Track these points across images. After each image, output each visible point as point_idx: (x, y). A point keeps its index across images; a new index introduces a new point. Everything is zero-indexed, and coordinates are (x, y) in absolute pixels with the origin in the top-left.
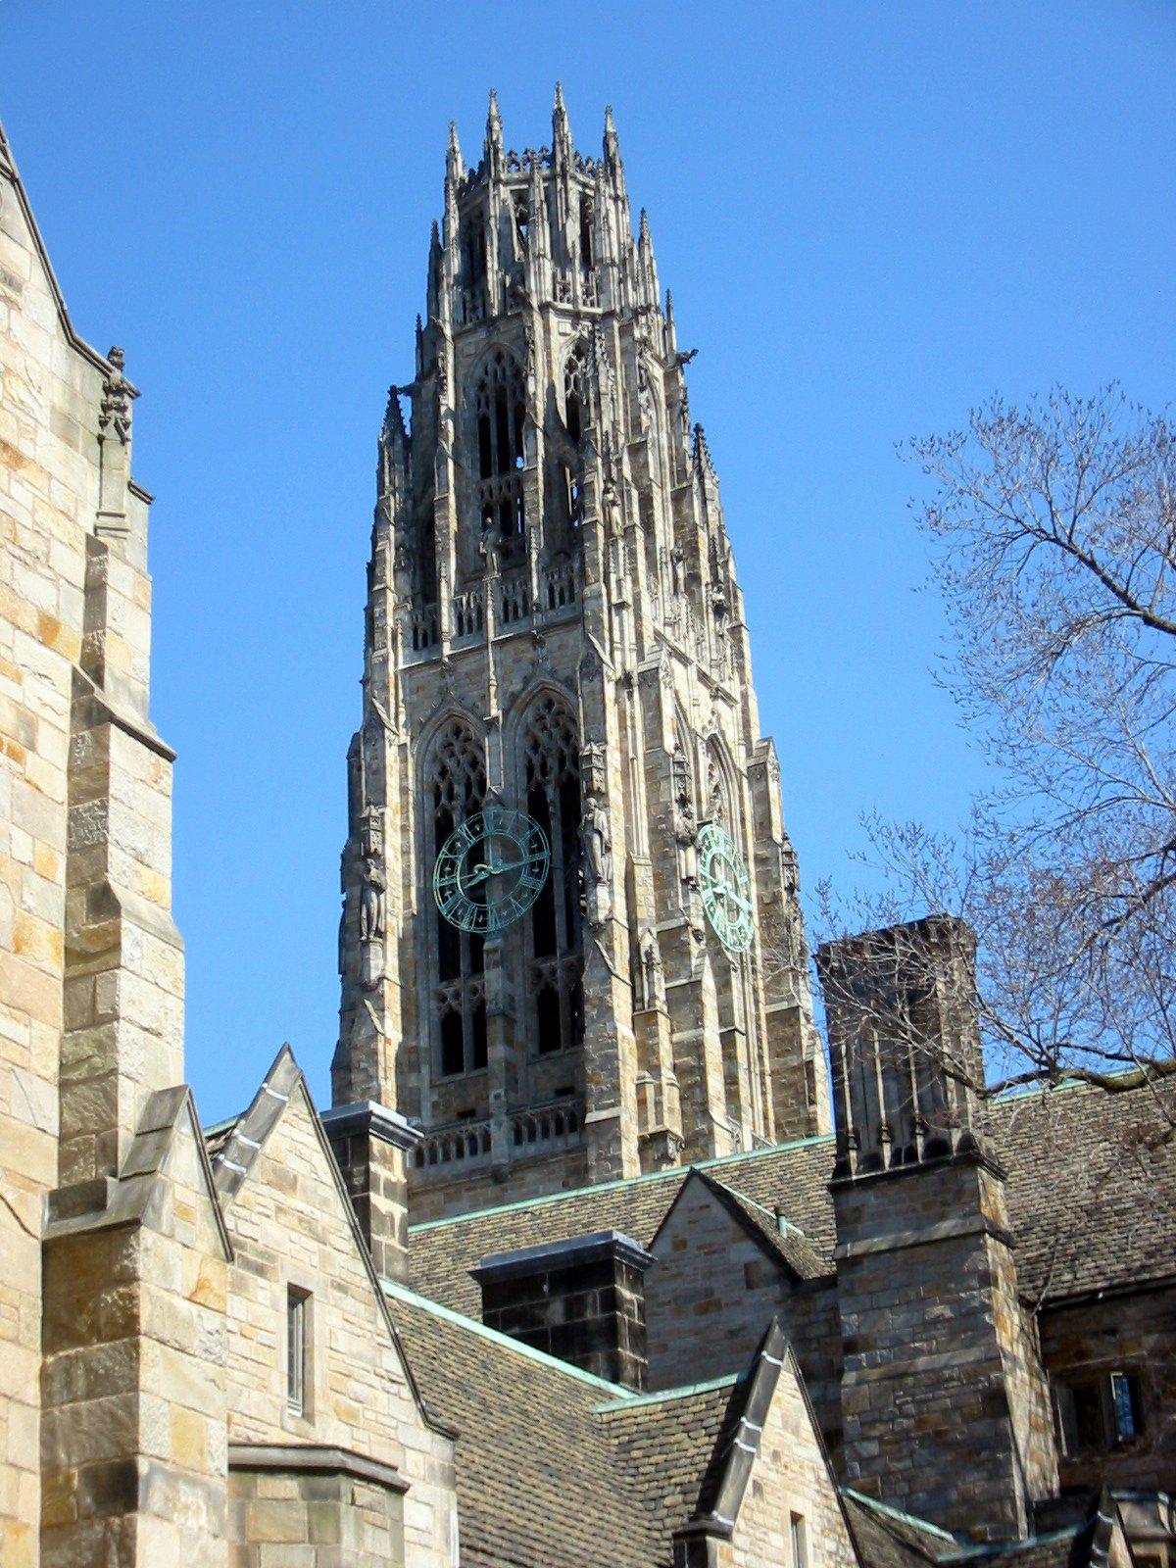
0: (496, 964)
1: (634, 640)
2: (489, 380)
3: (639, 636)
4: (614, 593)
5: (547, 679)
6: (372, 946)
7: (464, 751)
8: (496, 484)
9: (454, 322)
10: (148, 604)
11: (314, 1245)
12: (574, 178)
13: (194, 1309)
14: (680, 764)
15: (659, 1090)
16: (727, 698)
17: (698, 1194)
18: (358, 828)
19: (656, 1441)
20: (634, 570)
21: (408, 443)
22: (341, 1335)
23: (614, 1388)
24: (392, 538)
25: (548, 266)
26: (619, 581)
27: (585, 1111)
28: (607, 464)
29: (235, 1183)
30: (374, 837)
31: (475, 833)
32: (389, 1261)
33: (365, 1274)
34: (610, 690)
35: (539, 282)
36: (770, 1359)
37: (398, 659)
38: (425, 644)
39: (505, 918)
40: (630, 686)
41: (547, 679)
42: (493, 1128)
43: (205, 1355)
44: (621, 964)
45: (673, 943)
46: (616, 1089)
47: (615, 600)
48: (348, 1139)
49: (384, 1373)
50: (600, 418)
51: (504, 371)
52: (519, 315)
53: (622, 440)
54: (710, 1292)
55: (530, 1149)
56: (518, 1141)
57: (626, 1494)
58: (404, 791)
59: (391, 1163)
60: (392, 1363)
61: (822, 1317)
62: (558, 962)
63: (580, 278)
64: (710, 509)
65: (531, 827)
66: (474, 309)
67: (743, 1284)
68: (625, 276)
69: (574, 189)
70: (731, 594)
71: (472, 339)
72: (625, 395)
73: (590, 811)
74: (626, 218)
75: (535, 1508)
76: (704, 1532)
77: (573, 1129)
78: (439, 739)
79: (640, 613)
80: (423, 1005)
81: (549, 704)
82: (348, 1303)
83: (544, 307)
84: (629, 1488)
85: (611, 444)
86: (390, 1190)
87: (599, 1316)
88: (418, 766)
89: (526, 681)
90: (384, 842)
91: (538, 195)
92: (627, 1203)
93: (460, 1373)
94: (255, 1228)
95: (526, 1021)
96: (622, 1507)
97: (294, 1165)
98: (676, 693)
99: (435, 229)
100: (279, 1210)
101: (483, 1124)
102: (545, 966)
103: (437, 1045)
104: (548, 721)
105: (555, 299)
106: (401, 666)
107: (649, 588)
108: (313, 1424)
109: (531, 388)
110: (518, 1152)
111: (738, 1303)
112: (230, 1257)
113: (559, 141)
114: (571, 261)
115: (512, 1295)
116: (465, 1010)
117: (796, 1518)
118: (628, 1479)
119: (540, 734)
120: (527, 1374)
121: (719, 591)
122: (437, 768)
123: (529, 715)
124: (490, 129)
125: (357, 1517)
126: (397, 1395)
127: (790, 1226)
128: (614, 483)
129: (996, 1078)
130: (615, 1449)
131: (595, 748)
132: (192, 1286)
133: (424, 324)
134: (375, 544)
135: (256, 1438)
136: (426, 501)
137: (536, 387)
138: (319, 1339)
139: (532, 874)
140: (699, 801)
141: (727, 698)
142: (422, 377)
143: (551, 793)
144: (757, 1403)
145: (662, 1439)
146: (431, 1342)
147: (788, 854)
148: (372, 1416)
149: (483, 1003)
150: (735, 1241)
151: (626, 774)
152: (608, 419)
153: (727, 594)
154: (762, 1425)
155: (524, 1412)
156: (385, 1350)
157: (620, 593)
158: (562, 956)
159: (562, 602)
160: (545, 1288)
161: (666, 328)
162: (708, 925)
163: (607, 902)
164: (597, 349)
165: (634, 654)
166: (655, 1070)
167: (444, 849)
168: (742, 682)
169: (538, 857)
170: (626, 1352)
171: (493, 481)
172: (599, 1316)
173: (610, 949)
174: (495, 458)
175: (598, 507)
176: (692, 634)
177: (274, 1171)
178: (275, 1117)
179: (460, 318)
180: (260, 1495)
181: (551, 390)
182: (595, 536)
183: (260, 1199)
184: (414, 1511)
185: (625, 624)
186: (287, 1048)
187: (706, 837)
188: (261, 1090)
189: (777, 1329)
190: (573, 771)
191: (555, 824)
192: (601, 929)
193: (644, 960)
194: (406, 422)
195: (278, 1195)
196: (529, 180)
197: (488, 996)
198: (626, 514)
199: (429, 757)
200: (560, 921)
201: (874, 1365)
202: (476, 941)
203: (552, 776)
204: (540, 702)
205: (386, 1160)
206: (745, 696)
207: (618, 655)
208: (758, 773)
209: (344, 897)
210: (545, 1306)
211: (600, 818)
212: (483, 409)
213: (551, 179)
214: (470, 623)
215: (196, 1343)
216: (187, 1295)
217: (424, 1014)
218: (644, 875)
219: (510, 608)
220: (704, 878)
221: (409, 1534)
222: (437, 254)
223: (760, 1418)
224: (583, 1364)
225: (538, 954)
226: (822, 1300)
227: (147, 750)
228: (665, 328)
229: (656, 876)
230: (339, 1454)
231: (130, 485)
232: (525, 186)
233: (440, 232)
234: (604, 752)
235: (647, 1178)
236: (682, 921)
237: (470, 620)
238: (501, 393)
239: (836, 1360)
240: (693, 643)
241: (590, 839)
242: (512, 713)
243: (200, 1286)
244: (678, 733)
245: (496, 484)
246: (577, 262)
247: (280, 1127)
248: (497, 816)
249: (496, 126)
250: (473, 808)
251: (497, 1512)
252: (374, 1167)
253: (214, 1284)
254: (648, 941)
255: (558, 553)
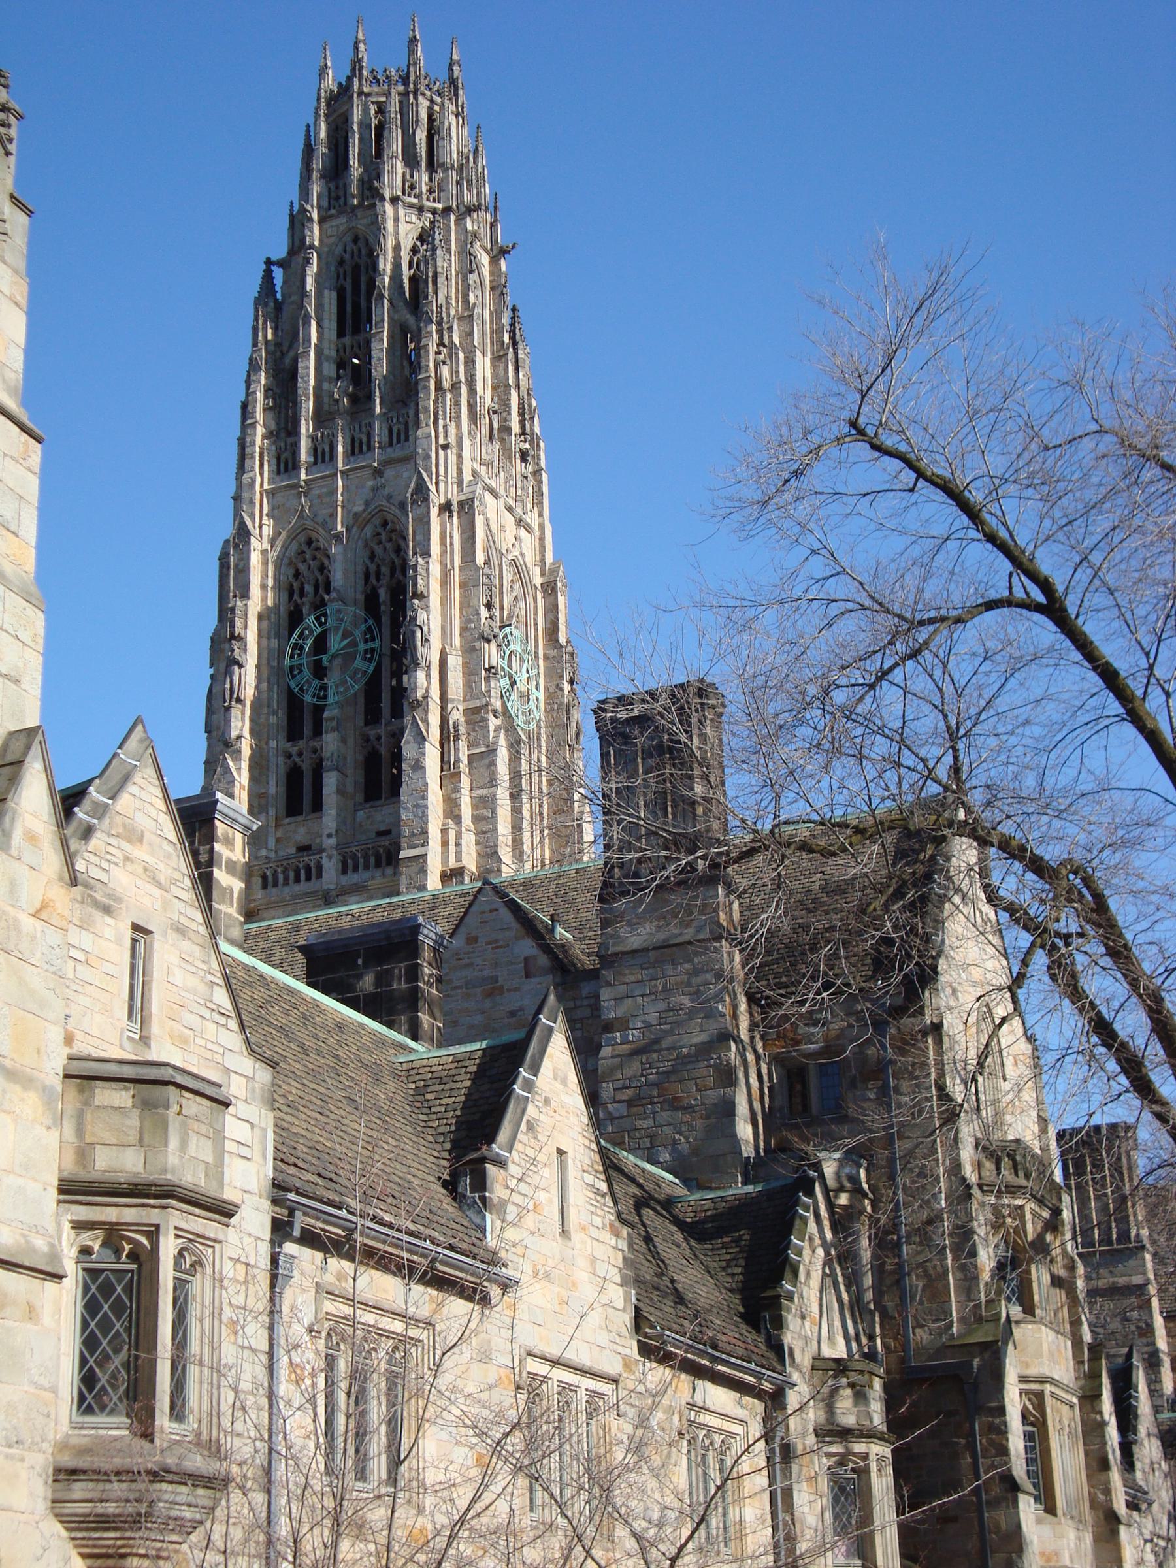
0: (333, 730)
1: (455, 475)
2: (347, 257)
3: (460, 471)
4: (441, 436)
5: (384, 503)
6: (233, 711)
7: (314, 558)
8: (348, 351)
9: (319, 208)
10: (24, 302)
11: (157, 892)
12: (423, 94)
13: (39, 924)
14: (489, 576)
15: (459, 835)
16: (528, 528)
17: (489, 896)
18: (226, 614)
19: (447, 1087)
20: (458, 418)
21: (279, 307)
22: (177, 971)
23: (412, 1044)
24: (263, 382)
25: (399, 166)
26: (445, 426)
27: (399, 849)
28: (440, 332)
29: (87, 833)
30: (238, 622)
31: (321, 624)
32: (227, 927)
33: (201, 920)
34: (434, 512)
35: (391, 179)
36: (544, 1020)
37: (262, 478)
38: (286, 470)
39: (341, 690)
40: (451, 512)
41: (384, 503)
42: (325, 861)
43: (46, 967)
44: (434, 734)
45: (476, 716)
46: (424, 832)
47: (441, 441)
48: (196, 820)
49: (215, 1007)
50: (436, 293)
51: (360, 251)
52: (374, 205)
53: (453, 312)
54: (495, 979)
55: (354, 878)
56: (344, 871)
57: (419, 1129)
58: (264, 587)
59: (233, 845)
60: (222, 998)
61: (585, 1002)
62: (382, 730)
63: (425, 178)
64: (521, 374)
65: (366, 621)
66: (337, 198)
67: (523, 974)
68: (462, 179)
69: (424, 103)
70: (534, 441)
71: (334, 222)
72: (457, 275)
73: (414, 610)
74: (465, 131)
75: (341, 1134)
76: (483, 1160)
77: (389, 863)
78: (294, 546)
79: (459, 455)
80: (273, 759)
81: (385, 524)
82: (186, 945)
83: (395, 200)
84: (422, 1124)
85: (444, 315)
86: (231, 867)
87: (404, 986)
88: (277, 569)
89: (367, 504)
90: (246, 628)
91: (394, 108)
92: (431, 909)
93: (284, 1021)
94: (104, 873)
95: (355, 776)
96: (415, 1139)
97: (143, 822)
98: (487, 520)
99: (308, 131)
100: (127, 859)
101: (317, 857)
102: (372, 733)
103: (282, 789)
104: (383, 537)
105: (404, 194)
106: (266, 486)
107: (469, 433)
108: (149, 1047)
109: (381, 266)
110: (344, 880)
111: (517, 989)
112: (74, 881)
113: (412, 62)
114: (418, 163)
115: (329, 965)
116: (306, 766)
117: (560, 1152)
118: (422, 1117)
119: (376, 547)
120: (341, 1026)
121: (525, 441)
122: (291, 572)
123: (368, 531)
124: (357, 48)
125: (184, 1125)
126: (226, 1026)
127: (563, 931)
128: (445, 346)
129: (742, 798)
130: (412, 1092)
131: (420, 560)
132: (38, 905)
133: (296, 208)
134: (248, 386)
135: (96, 1053)
136: (292, 354)
137: (385, 265)
138: (157, 974)
139: (365, 659)
140: (502, 608)
141: (528, 528)
142: (292, 252)
143: (383, 594)
144: (533, 1056)
145: (452, 1085)
146: (260, 994)
147: (572, 654)
148: (203, 1043)
149: (321, 760)
150: (517, 938)
151: (445, 582)
152: (444, 294)
153: (532, 443)
154: (536, 1075)
155: (337, 1057)
156: (215, 987)
157: (446, 436)
158: (386, 725)
159: (399, 442)
160: (360, 962)
161: (493, 225)
162: (504, 705)
163: (425, 682)
164: (437, 236)
165: (455, 486)
166: (458, 819)
167: (295, 636)
168: (541, 515)
169: (370, 645)
170: (424, 1018)
171: (347, 340)
172: (404, 986)
173: (426, 721)
174: (349, 322)
175: (431, 365)
176: (502, 473)
177: (124, 825)
178: (126, 779)
179: (326, 204)
180: (97, 1104)
181: (397, 266)
182: (427, 388)
183: (110, 849)
184: (234, 1128)
185: (449, 461)
186: (138, 721)
187: (506, 636)
188: (115, 755)
189: (552, 998)
190: (401, 578)
191: (386, 620)
192: (420, 705)
193: (452, 730)
194: (278, 288)
195: (125, 845)
196: (388, 94)
197: (326, 754)
198: (454, 372)
199: (286, 561)
200: (386, 697)
201: (625, 1042)
202: (319, 710)
203: (384, 582)
204: (377, 521)
205: (229, 842)
206: (542, 527)
207: (442, 485)
208: (550, 589)
209: (212, 671)
210: (359, 977)
211: (421, 616)
212: (342, 280)
213: (405, 94)
214: (323, 454)
215: (38, 955)
216: (32, 911)
217: (273, 767)
218: (455, 662)
219: (357, 444)
220: (503, 669)
221: (229, 1146)
222: (309, 150)
223: (535, 1069)
224: (390, 1025)
225: (366, 724)
226: (586, 989)
227: (18, 430)
228: (492, 225)
229: (465, 664)
230: (170, 1071)
231: (12, 196)
232: (384, 99)
233: (312, 133)
234: (428, 563)
235: (447, 890)
236: (484, 701)
237: (323, 453)
238: (356, 269)
239: (596, 1038)
240: (502, 481)
241: (413, 632)
242: (355, 529)
243: (44, 906)
244: (487, 550)
245: (348, 351)
246: (423, 164)
247: (131, 788)
248: (339, 611)
249: (362, 47)
250: (319, 606)
251: (309, 1135)
252: (217, 847)
253: (58, 905)
254: (457, 716)
255: (397, 402)
